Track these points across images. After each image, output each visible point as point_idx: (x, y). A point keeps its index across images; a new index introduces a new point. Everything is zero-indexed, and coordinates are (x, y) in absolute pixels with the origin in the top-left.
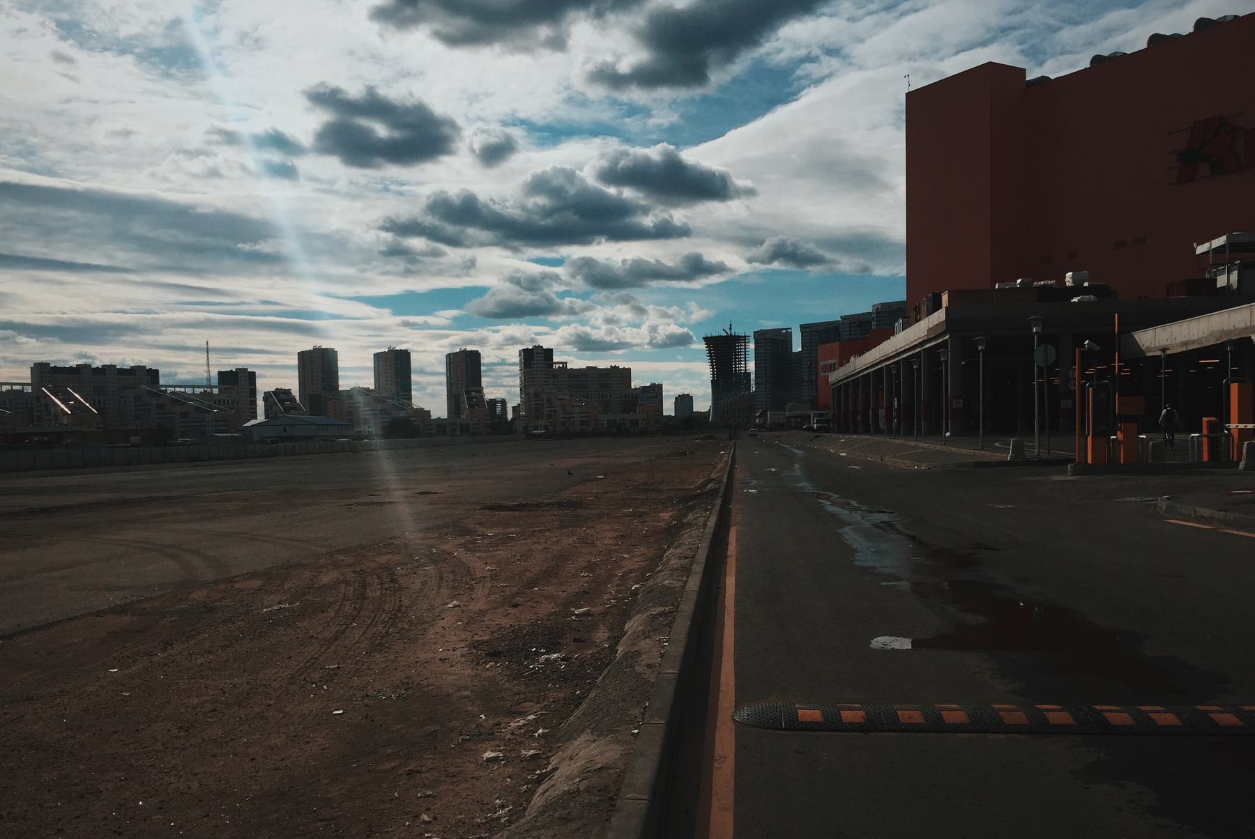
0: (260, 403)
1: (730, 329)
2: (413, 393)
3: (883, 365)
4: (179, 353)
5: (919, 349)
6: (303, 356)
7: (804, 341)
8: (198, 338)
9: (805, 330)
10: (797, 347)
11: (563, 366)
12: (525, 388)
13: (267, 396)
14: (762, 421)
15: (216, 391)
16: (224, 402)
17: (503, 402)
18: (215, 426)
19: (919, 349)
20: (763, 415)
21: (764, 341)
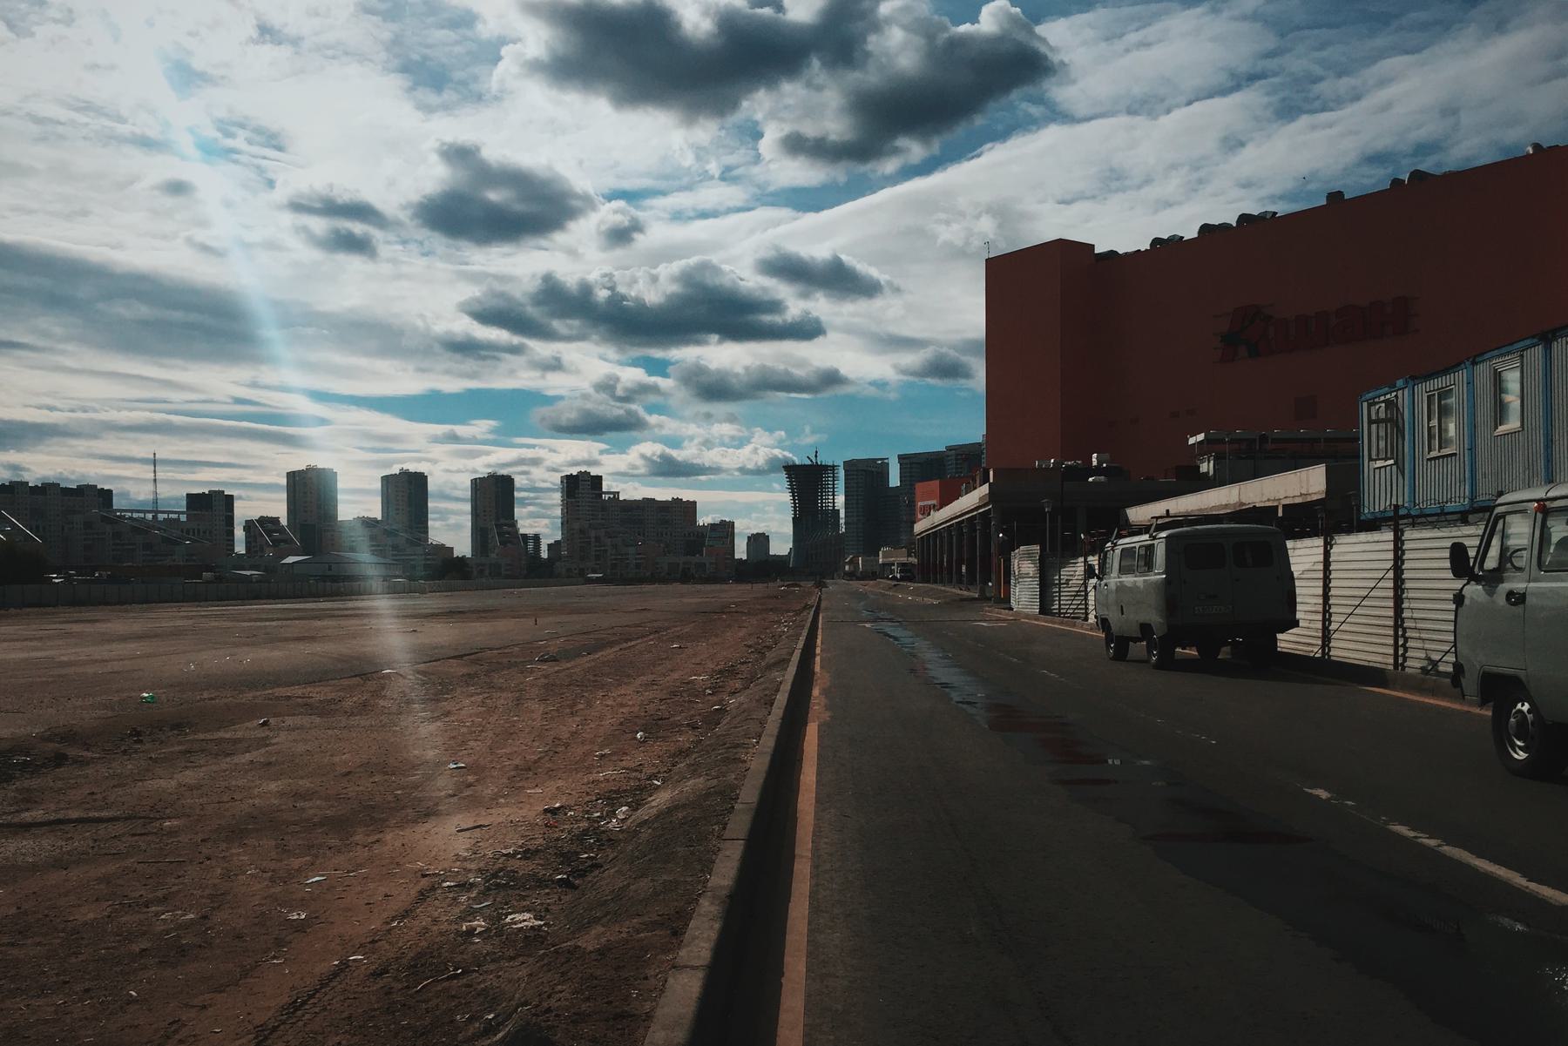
0: (239, 533)
1: (816, 456)
2: (430, 523)
3: (954, 522)
4: (120, 465)
5: (975, 513)
6: (292, 476)
7: (903, 479)
8: (142, 447)
9: (905, 461)
10: (894, 480)
11: (614, 496)
12: (567, 522)
13: (249, 526)
14: (852, 569)
15: (183, 518)
16: (194, 533)
17: (537, 538)
18: (187, 560)
19: (975, 513)
20: (853, 562)
21: (855, 473)
